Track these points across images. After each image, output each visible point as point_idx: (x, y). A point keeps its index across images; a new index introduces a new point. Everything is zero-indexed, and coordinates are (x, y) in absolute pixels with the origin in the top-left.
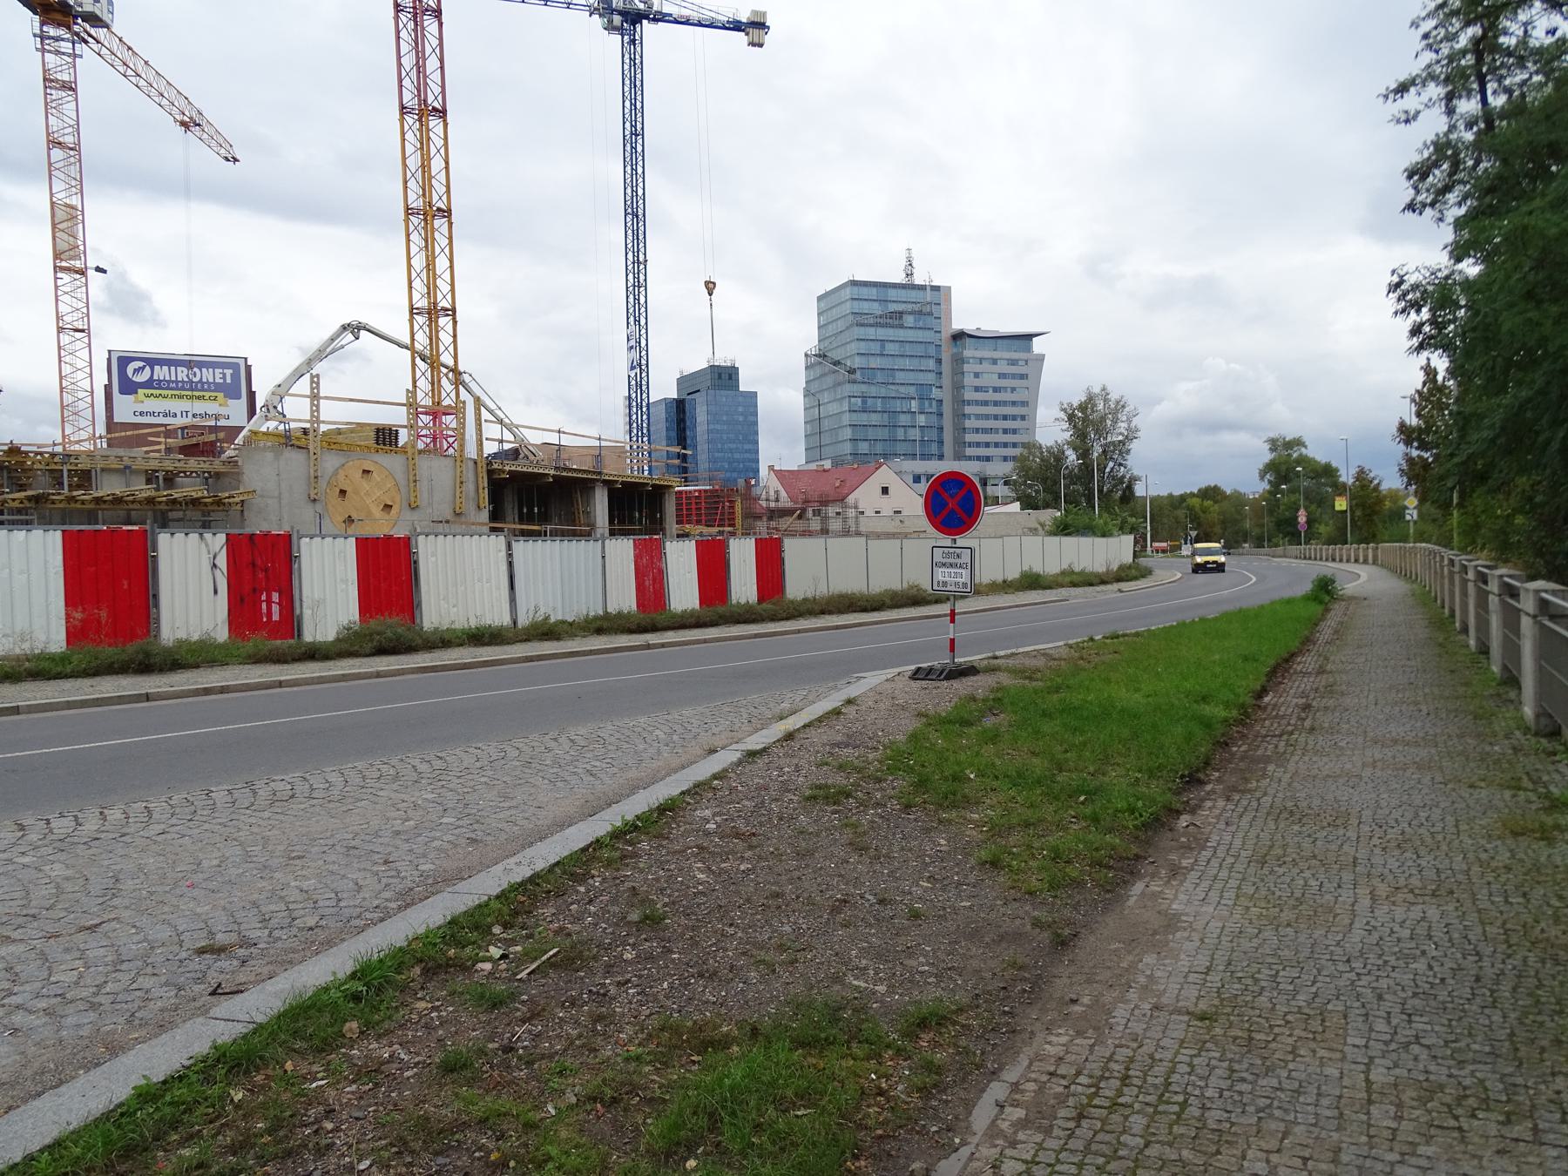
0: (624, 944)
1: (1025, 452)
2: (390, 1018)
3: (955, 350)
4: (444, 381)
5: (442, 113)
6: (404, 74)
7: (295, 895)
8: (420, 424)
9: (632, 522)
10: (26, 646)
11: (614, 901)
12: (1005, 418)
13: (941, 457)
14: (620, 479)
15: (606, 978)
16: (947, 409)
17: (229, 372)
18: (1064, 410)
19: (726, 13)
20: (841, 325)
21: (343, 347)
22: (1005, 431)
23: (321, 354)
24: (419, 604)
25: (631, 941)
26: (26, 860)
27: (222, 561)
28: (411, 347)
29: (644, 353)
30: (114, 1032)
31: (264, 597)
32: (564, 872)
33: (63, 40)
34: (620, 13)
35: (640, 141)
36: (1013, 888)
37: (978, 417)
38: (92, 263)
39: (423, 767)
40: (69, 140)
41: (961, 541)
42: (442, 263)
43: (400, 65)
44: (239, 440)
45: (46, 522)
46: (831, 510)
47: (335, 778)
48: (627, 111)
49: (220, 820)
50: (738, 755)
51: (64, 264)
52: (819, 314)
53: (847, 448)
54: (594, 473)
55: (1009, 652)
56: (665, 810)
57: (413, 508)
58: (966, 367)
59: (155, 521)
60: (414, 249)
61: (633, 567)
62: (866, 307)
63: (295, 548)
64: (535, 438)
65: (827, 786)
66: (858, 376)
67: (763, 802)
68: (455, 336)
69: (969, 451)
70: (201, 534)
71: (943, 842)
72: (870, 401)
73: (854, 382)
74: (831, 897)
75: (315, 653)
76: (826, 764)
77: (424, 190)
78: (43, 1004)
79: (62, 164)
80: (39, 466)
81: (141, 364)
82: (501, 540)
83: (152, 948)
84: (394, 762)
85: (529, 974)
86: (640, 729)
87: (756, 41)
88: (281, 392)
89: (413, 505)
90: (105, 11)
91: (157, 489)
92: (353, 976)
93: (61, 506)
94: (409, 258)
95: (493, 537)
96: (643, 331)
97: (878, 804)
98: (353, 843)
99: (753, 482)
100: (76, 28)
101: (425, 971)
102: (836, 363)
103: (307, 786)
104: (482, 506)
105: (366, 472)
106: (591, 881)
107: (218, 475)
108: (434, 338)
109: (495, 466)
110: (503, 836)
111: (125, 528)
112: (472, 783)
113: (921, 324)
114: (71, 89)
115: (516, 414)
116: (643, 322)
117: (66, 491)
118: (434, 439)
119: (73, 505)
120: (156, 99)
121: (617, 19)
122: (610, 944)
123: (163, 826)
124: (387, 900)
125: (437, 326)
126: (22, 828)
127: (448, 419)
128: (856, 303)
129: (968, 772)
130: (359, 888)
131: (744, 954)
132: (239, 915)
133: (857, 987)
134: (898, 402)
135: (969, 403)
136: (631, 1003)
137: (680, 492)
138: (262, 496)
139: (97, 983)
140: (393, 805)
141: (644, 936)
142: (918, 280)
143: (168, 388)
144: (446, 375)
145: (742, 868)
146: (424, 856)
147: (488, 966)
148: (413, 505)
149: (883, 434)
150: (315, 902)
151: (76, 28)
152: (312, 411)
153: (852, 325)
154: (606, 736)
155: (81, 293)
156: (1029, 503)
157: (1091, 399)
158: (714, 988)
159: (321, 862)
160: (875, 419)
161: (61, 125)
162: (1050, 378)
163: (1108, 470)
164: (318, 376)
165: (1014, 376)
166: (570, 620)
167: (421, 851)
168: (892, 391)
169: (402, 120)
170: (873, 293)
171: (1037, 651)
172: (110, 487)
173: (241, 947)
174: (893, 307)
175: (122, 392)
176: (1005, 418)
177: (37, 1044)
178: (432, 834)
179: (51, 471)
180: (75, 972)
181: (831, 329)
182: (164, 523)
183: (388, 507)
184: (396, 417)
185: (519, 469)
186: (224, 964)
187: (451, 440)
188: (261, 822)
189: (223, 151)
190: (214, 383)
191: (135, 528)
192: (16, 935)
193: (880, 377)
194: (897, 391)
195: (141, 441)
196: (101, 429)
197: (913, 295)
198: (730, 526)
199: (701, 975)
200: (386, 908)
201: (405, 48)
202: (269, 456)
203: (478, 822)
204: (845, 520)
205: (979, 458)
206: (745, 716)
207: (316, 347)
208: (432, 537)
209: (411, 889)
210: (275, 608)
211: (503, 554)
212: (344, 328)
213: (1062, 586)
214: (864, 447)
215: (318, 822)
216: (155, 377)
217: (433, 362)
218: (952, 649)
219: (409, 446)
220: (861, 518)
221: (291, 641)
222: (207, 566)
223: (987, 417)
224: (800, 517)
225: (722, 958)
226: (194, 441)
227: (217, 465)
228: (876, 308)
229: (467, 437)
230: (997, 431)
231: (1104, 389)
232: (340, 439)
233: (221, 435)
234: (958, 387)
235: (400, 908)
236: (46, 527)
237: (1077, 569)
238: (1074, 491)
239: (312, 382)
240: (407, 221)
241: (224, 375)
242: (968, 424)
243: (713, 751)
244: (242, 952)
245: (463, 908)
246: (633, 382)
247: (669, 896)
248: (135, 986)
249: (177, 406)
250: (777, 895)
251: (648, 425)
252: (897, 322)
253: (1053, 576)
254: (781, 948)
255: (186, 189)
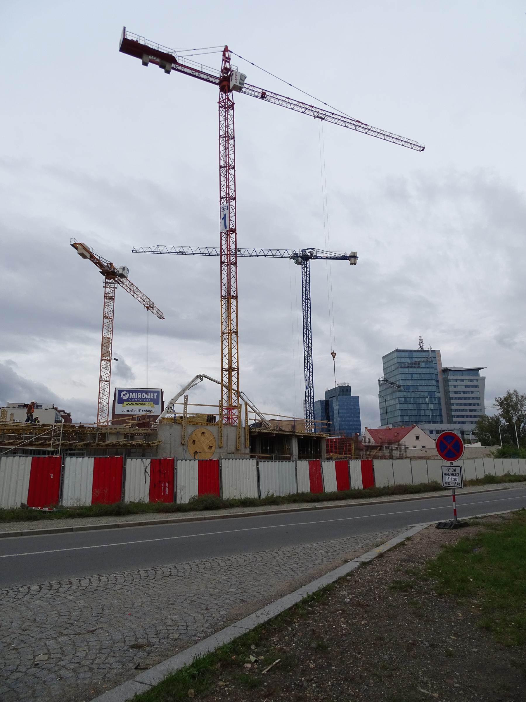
0: (310, 659)
1: (481, 420)
2: (207, 689)
3: (444, 376)
4: (234, 396)
5: (236, 297)
6: (223, 285)
7: (170, 622)
8: (224, 413)
9: (308, 453)
10: (78, 503)
11: (304, 636)
12: (470, 404)
13: (442, 422)
14: (303, 435)
15: (302, 677)
16: (443, 401)
17: (155, 394)
18: (497, 401)
19: (342, 254)
20: (393, 368)
21: (196, 384)
22: (470, 410)
23: (189, 386)
24: (222, 487)
25: (313, 658)
26: (71, 598)
27: (149, 470)
28: (221, 383)
29: (311, 382)
30: (97, 683)
31: (163, 485)
32: (282, 620)
33: (112, 283)
34: (301, 257)
35: (309, 302)
36: (499, 642)
37: (458, 404)
38: (113, 357)
39: (222, 564)
40: (110, 316)
41: (455, 463)
42: (234, 351)
43: (221, 282)
44: (157, 421)
45: (89, 455)
46: (394, 447)
47: (187, 567)
48: (304, 291)
49: (142, 584)
50: (358, 564)
51: (104, 358)
52: (384, 364)
53: (399, 419)
54: (292, 432)
55: (483, 515)
56: (326, 590)
57: (220, 448)
58: (450, 383)
59: (126, 454)
60: (224, 347)
61: (308, 473)
62: (403, 360)
63: (175, 464)
64: (268, 418)
65: (400, 582)
66: (402, 388)
67: (371, 589)
68: (238, 379)
69: (454, 420)
70: (142, 459)
71: (460, 615)
72: (408, 399)
73: (400, 391)
74: (406, 641)
75: (181, 509)
76: (400, 570)
77: (228, 325)
78: (72, 666)
79: (107, 324)
80: (89, 432)
81: (126, 392)
82: (254, 461)
83: (114, 643)
84: (210, 560)
85: (267, 671)
86: (313, 549)
87: (353, 262)
88: (173, 402)
89: (220, 446)
90: (126, 273)
91: (127, 441)
92: (192, 666)
93: (94, 447)
94: (222, 350)
95: (251, 460)
96: (311, 374)
97: (426, 593)
98: (194, 599)
99: (358, 434)
100: (116, 279)
101: (223, 666)
102: (392, 383)
103: (176, 570)
104: (247, 446)
105: (203, 433)
106: (294, 625)
107: (149, 435)
108: (230, 380)
109: (252, 430)
110: (255, 600)
111: (116, 457)
112: (242, 573)
113: (428, 366)
114: (113, 299)
115: (261, 409)
116: (311, 370)
117: (97, 442)
118: (229, 419)
119: (98, 447)
120: (139, 300)
121: (300, 260)
122: (303, 659)
123: (121, 586)
124: (207, 628)
125: (231, 375)
126: (70, 583)
127: (235, 411)
128: (399, 359)
129: (469, 577)
130: (196, 621)
131: (366, 669)
132: (148, 630)
133: (424, 693)
134: (420, 399)
135: (452, 398)
136: (314, 691)
137: (328, 440)
138: (164, 443)
139: (93, 658)
140: (210, 581)
141: (318, 656)
142: (426, 348)
143: (134, 401)
144: (234, 394)
145: (363, 622)
146: (222, 607)
147: (249, 666)
148: (220, 446)
149: (415, 413)
150: (178, 627)
151: (116, 279)
152: (184, 410)
153: (398, 368)
154: (299, 552)
155: (108, 368)
156: (485, 443)
157: (509, 396)
158: (353, 687)
159: (180, 607)
160: (411, 406)
161: (108, 311)
162: (488, 387)
163: (521, 427)
164: (187, 396)
165: (472, 387)
166: (282, 496)
167: (221, 604)
168: (417, 394)
169: (222, 301)
170: (406, 354)
171: (497, 515)
172: (112, 440)
173: (148, 646)
174: (415, 360)
175: (119, 403)
176: (470, 404)
177: (69, 686)
178: (226, 596)
179: (92, 434)
180: (85, 652)
181: (389, 370)
182: (129, 454)
183: (210, 447)
184: (215, 411)
185: (262, 431)
186: (142, 654)
187: (235, 419)
188: (158, 586)
189: (159, 316)
190: (150, 398)
191: (119, 457)
192: (65, 632)
193: (411, 389)
194: (420, 394)
195: (124, 422)
196: (110, 418)
197: (424, 354)
198: (349, 454)
199: (346, 680)
200: (206, 632)
201: (223, 276)
202: (168, 427)
203: (245, 592)
204: (400, 451)
205: (459, 423)
206: (360, 544)
207: (186, 384)
208: (227, 460)
209: (217, 623)
210: (167, 489)
211: (255, 467)
212: (197, 377)
213: (505, 482)
214: (406, 419)
215: (180, 587)
216: (130, 397)
217: (230, 388)
218: (455, 514)
219: (220, 422)
220: (408, 450)
221: (172, 503)
222: (143, 472)
223: (461, 404)
224: (380, 450)
225: (356, 671)
226: (142, 422)
227: (149, 431)
228: (408, 360)
229: (242, 418)
230: (466, 410)
231: (515, 391)
232: (194, 420)
233: (151, 419)
234: (447, 392)
235: (212, 632)
236: (89, 456)
237: (512, 474)
238: (506, 436)
239: (185, 398)
240: (222, 336)
241: (154, 395)
242: (453, 408)
243: (346, 562)
244: (148, 649)
245: (238, 635)
246: (307, 394)
247: (330, 635)
248: (106, 661)
249: (136, 408)
250: (380, 639)
251: (314, 411)
252: (417, 366)
253: (501, 477)
254: (384, 668)
255: (147, 330)
